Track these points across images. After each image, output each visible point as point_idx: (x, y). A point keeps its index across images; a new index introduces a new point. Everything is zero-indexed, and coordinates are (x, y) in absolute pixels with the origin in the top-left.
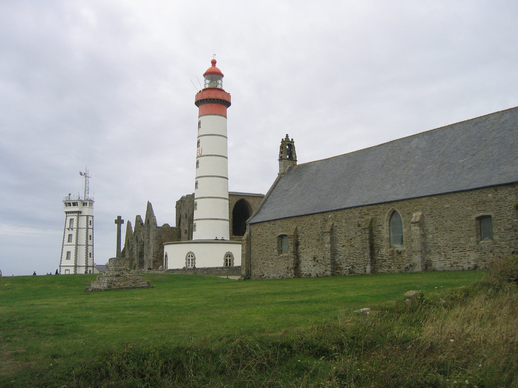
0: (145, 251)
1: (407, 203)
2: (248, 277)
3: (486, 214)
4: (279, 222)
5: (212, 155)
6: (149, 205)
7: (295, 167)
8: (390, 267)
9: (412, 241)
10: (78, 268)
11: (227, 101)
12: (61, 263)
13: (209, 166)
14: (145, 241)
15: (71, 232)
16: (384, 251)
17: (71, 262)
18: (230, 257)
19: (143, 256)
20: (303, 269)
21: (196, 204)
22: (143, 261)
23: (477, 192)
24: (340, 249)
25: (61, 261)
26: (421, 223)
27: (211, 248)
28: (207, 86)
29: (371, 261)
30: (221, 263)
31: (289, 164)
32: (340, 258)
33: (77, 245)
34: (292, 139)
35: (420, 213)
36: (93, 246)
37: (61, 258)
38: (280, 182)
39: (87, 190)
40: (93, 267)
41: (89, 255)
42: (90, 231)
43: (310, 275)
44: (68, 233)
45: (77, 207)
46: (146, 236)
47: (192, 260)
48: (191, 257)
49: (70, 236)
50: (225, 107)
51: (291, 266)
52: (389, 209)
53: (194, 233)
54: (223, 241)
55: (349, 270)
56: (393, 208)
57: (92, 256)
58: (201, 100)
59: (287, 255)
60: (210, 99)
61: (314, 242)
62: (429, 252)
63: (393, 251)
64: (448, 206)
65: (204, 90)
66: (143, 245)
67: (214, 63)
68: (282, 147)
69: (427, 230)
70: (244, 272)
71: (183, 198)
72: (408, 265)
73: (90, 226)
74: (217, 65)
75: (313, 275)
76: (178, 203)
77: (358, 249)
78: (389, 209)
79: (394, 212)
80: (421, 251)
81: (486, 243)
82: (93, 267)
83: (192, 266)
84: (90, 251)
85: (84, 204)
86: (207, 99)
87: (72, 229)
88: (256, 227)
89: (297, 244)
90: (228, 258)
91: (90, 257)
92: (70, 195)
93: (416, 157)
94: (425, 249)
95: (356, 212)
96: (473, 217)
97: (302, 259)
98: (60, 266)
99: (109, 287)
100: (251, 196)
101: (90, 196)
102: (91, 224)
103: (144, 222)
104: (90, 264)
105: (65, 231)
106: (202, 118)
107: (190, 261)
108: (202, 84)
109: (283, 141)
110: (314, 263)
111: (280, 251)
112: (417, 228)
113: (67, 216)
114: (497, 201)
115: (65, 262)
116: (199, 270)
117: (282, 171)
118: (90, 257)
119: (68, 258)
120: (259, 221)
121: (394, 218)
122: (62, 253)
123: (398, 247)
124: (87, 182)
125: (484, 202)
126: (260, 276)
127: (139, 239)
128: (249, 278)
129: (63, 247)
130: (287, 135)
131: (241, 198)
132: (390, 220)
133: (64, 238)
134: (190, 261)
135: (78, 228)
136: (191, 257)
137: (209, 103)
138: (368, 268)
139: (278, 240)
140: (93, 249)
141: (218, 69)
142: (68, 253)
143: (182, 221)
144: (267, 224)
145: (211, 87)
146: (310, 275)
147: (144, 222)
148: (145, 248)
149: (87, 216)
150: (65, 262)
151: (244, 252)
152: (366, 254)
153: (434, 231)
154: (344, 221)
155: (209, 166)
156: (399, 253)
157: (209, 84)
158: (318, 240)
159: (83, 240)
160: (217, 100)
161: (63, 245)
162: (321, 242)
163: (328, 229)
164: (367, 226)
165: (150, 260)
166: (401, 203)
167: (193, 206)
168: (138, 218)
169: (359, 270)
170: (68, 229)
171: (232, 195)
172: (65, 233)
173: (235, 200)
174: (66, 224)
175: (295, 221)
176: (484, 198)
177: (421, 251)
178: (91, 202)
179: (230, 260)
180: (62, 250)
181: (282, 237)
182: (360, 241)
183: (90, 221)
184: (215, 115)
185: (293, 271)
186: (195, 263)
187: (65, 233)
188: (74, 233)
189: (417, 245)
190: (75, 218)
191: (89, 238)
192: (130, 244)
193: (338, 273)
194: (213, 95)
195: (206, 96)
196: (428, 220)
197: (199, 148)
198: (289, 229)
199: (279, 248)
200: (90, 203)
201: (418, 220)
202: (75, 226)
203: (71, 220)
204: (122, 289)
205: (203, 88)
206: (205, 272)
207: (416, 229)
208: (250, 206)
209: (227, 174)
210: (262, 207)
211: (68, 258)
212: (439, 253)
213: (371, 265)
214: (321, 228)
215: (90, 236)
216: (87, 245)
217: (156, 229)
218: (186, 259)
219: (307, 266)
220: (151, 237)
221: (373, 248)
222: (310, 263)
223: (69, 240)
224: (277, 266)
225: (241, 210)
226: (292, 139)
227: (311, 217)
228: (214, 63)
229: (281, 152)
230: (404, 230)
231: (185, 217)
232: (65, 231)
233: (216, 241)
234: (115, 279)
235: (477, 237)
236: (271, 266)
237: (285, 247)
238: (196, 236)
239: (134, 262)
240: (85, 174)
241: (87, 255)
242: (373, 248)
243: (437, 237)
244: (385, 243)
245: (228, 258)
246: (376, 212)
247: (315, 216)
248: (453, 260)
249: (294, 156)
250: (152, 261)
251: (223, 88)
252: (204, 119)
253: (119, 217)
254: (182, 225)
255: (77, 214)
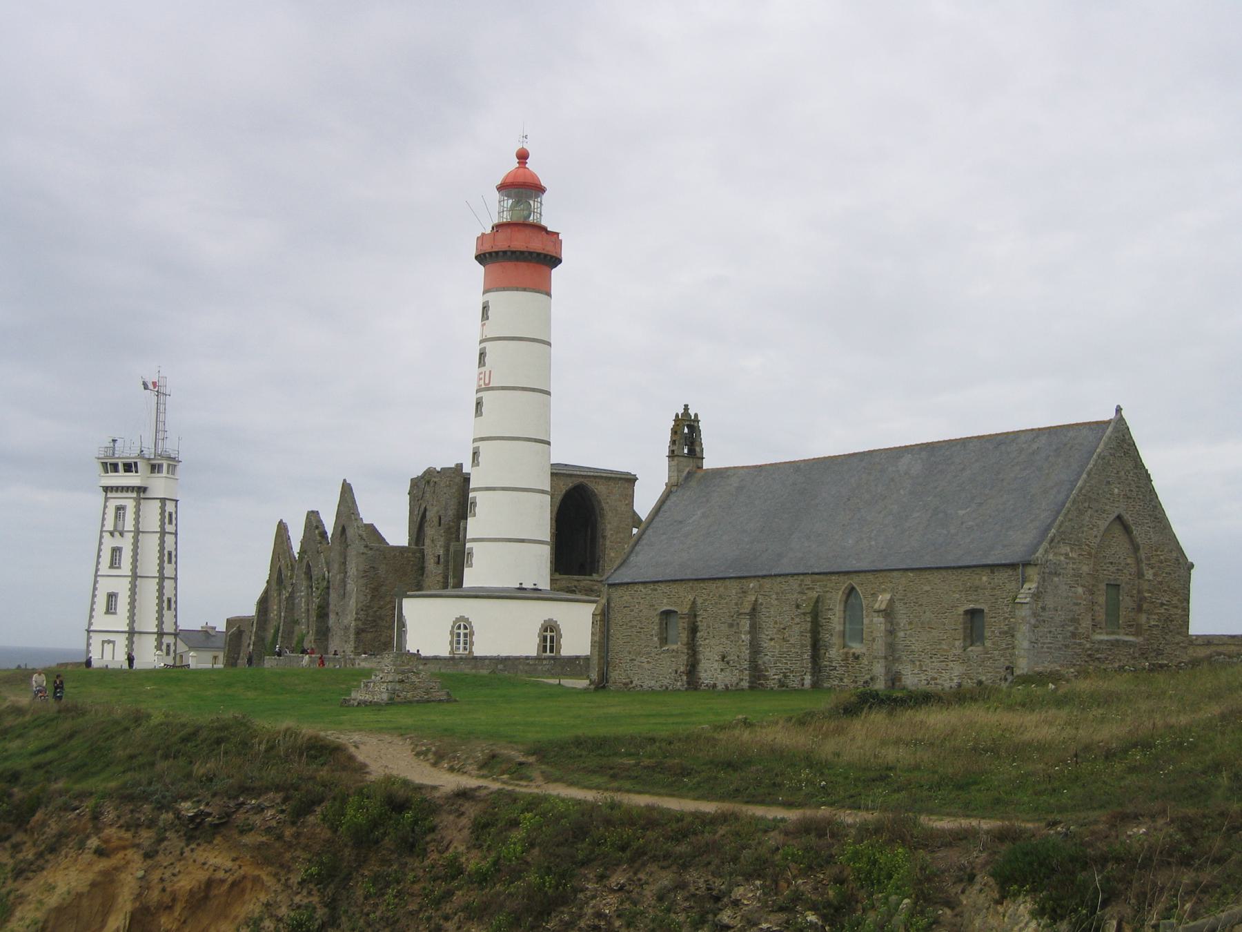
0: (331, 601)
1: (870, 577)
2: (601, 685)
3: (978, 607)
4: (663, 586)
5: (516, 379)
6: (347, 490)
7: (700, 473)
8: (841, 679)
9: (874, 640)
10: (136, 638)
11: (552, 257)
12: (90, 624)
13: (505, 413)
14: (342, 584)
15: (117, 542)
16: (834, 654)
17: (120, 621)
18: (552, 631)
19: (327, 615)
20: (703, 675)
21: (474, 504)
22: (328, 629)
23: (968, 572)
24: (766, 644)
25: (91, 617)
26: (888, 613)
27: (498, 606)
28: (506, 218)
29: (813, 668)
30: (529, 648)
31: (688, 466)
32: (766, 659)
33: (135, 576)
34: (696, 415)
35: (888, 596)
36: (175, 579)
37: (92, 610)
38: (668, 503)
39: (159, 429)
40: (176, 635)
41: (166, 604)
42: (169, 539)
43: (715, 686)
44: (109, 543)
45: (136, 475)
46: (336, 566)
47: (465, 635)
48: (462, 630)
49: (116, 551)
50: (545, 268)
51: (682, 669)
52: (845, 583)
53: (466, 570)
54: (534, 594)
55: (780, 680)
56: (852, 583)
57: (173, 606)
58: (490, 253)
59: (675, 647)
60: (513, 252)
61: (724, 627)
62: (898, 660)
63: (847, 653)
64: (927, 588)
65: (498, 227)
66: (328, 588)
67: (523, 156)
68: (674, 432)
69: (898, 624)
70: (594, 675)
71: (430, 473)
72: (868, 677)
73: (169, 528)
74: (530, 164)
75: (720, 687)
76: (415, 483)
77: (794, 646)
78: (845, 583)
79: (852, 590)
80: (886, 658)
81: (975, 650)
82: (176, 635)
83: (465, 649)
84: (168, 593)
85: (155, 468)
86: (505, 252)
87: (122, 534)
88: (620, 591)
89: (694, 630)
90: (549, 634)
91: (169, 608)
92: (114, 441)
93: (902, 492)
94: (892, 654)
95: (794, 583)
96: (961, 610)
97: (701, 657)
98: (89, 631)
99: (391, 699)
100: (602, 477)
101: (170, 446)
102: (170, 522)
103: (330, 535)
104: (168, 627)
105: (101, 537)
106: (492, 296)
107: (462, 638)
108: (491, 210)
109: (677, 419)
110: (723, 665)
111: (664, 640)
112: (882, 619)
113: (107, 499)
114: (993, 589)
115: (102, 621)
116: (487, 662)
117: (674, 480)
118: (169, 608)
119: (110, 609)
120: (626, 580)
121: (852, 600)
122: (94, 596)
123: (857, 648)
124: (162, 407)
125: (976, 589)
126: (626, 684)
127: (315, 572)
128: (604, 687)
129: (96, 582)
130: (686, 406)
131: (577, 481)
132: (846, 602)
133: (99, 556)
134: (462, 638)
135: (137, 532)
136: (462, 630)
137: (510, 260)
138: (808, 680)
139: (661, 620)
140: (176, 588)
141: (534, 176)
142: (112, 597)
143: (430, 531)
144: (641, 587)
145: (515, 220)
146: (715, 686)
147: (330, 531)
148: (333, 596)
149: (163, 500)
150: (102, 621)
151: (597, 638)
152: (805, 656)
153: (908, 627)
154: (774, 596)
155: (505, 413)
156: (856, 657)
157: (512, 209)
158: (731, 626)
159: (150, 565)
160: (530, 253)
161: (96, 576)
162: (734, 629)
163: (747, 608)
164: (809, 610)
165: (346, 628)
166: (862, 575)
167: (463, 508)
168: (313, 521)
169: (794, 682)
170: (112, 534)
171: (559, 473)
172: (101, 543)
173: (564, 487)
174: (103, 519)
175: (692, 588)
176: (977, 582)
177: (886, 658)
178: (173, 462)
179: (552, 638)
180: (95, 589)
181: (667, 614)
182: (798, 632)
183: (170, 515)
184: (525, 290)
185: (685, 678)
186: (472, 643)
187: (101, 543)
188: (126, 544)
189: (879, 647)
190: (130, 505)
191: (166, 558)
192: (287, 582)
193: (761, 684)
194: (520, 242)
195: (502, 244)
196: (899, 606)
197: (483, 369)
198: (680, 601)
199: (661, 633)
200: (169, 465)
201: (883, 607)
202: (129, 524)
203: (119, 509)
204: (411, 702)
205: (496, 221)
206: (500, 667)
207: (879, 620)
208: (599, 502)
209: (548, 432)
210: (632, 552)
211: (110, 609)
212: (913, 662)
213: (813, 675)
214: (736, 604)
215: (170, 554)
216: (162, 578)
217: (365, 550)
218: (452, 633)
219: (710, 671)
220: (352, 570)
221: (817, 647)
222: (716, 665)
223: (114, 563)
224: (654, 667)
225: (582, 518)
226: (696, 415)
227: (719, 583)
228: (523, 156)
229: (673, 442)
230: (866, 621)
231: (436, 520)
232: (101, 537)
233: (521, 593)
234: (398, 687)
235: (965, 640)
236: (646, 666)
237: (672, 633)
238: (472, 578)
239: (297, 628)
240: (154, 384)
241: (160, 604)
242: (817, 647)
243: (911, 635)
244: (836, 640)
245: (549, 634)
246: (825, 586)
247: (727, 582)
248: (931, 673)
249: (698, 449)
250: (352, 630)
251: (543, 223)
252: (499, 299)
254: (427, 541)
255: (134, 495)
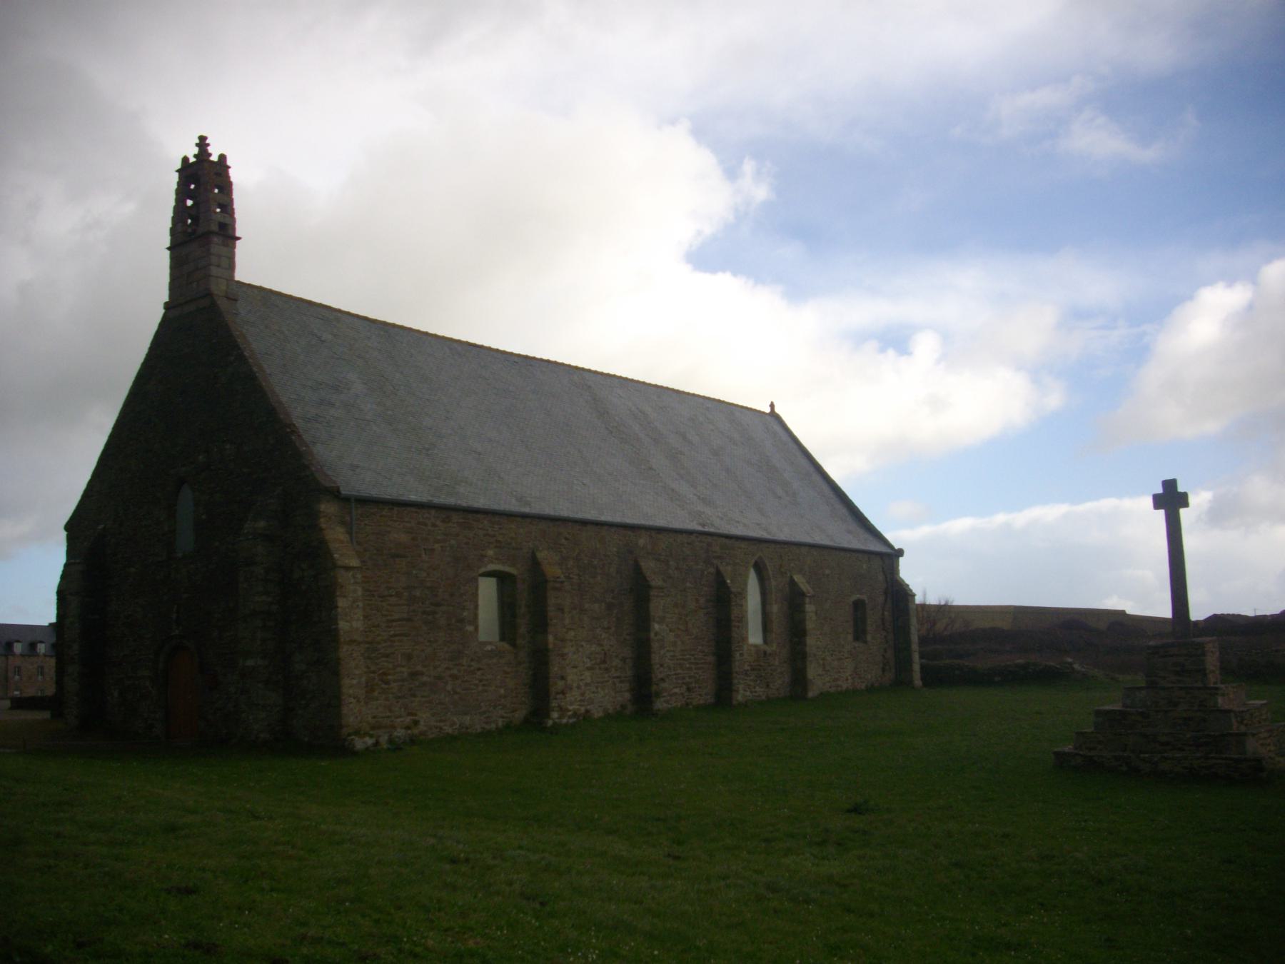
34: (223, 158)
208: (294, 431)
226: (223, 158)
253: (1170, 485)
